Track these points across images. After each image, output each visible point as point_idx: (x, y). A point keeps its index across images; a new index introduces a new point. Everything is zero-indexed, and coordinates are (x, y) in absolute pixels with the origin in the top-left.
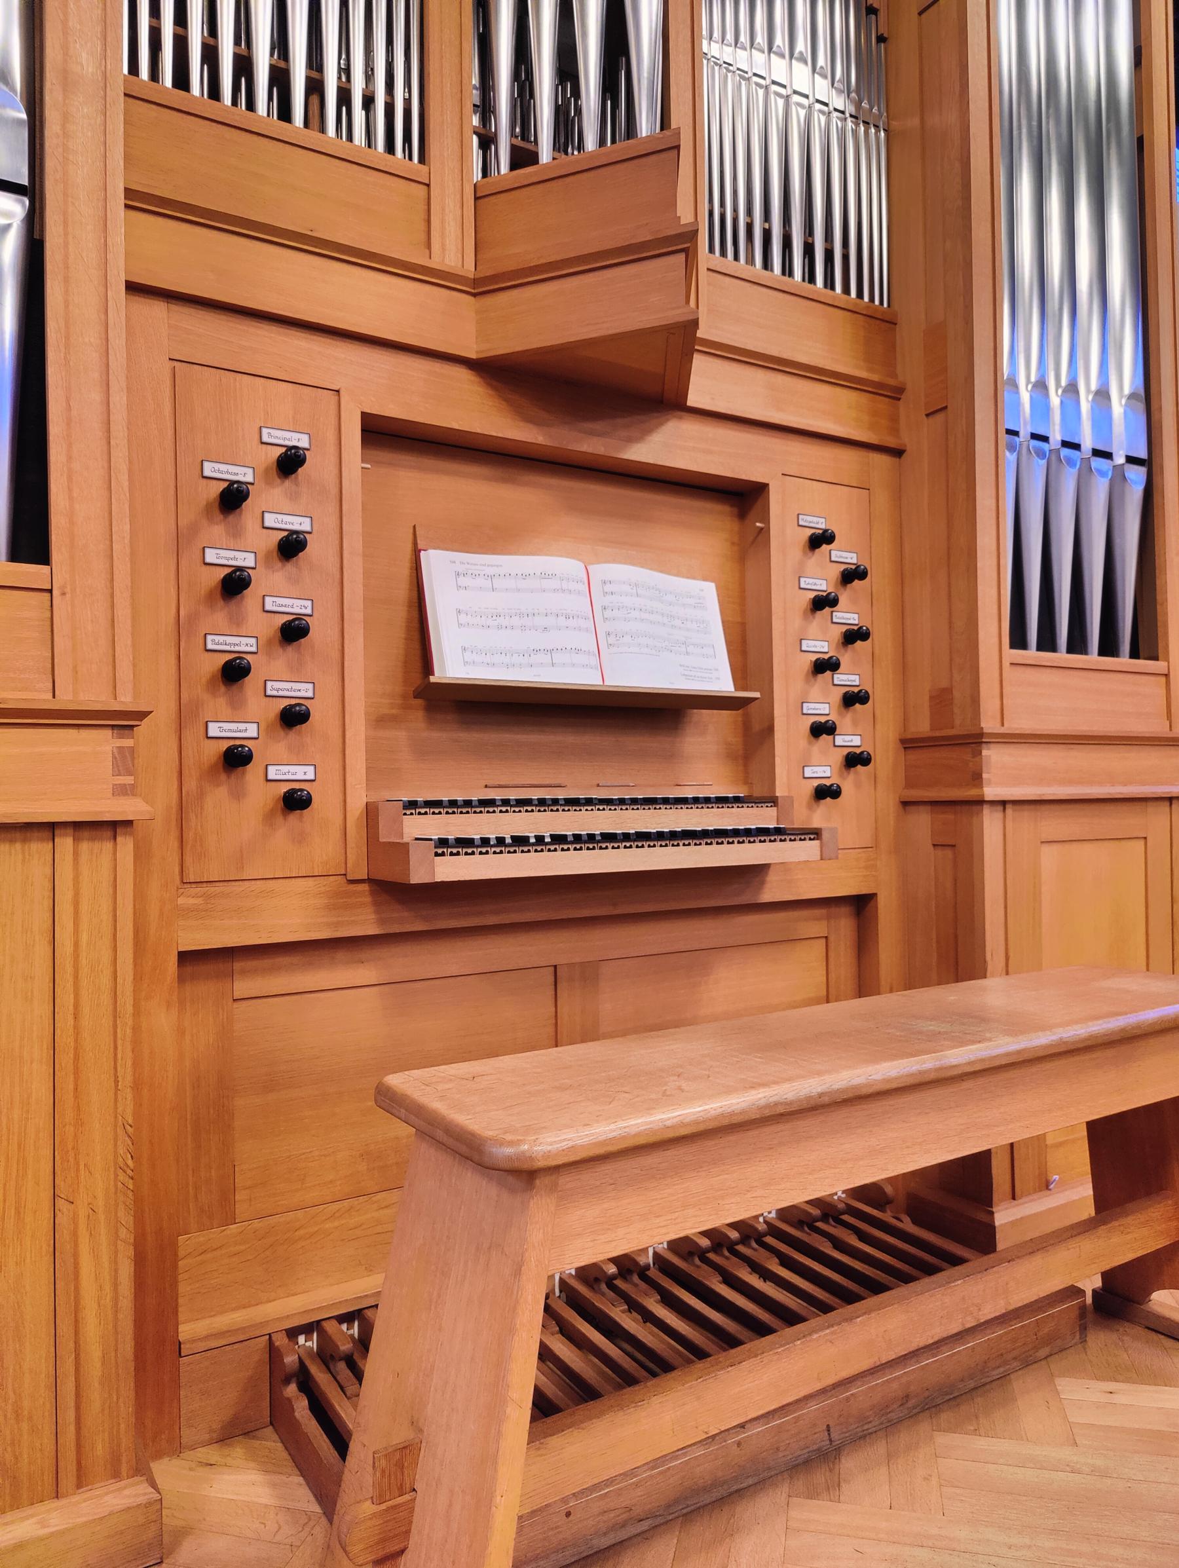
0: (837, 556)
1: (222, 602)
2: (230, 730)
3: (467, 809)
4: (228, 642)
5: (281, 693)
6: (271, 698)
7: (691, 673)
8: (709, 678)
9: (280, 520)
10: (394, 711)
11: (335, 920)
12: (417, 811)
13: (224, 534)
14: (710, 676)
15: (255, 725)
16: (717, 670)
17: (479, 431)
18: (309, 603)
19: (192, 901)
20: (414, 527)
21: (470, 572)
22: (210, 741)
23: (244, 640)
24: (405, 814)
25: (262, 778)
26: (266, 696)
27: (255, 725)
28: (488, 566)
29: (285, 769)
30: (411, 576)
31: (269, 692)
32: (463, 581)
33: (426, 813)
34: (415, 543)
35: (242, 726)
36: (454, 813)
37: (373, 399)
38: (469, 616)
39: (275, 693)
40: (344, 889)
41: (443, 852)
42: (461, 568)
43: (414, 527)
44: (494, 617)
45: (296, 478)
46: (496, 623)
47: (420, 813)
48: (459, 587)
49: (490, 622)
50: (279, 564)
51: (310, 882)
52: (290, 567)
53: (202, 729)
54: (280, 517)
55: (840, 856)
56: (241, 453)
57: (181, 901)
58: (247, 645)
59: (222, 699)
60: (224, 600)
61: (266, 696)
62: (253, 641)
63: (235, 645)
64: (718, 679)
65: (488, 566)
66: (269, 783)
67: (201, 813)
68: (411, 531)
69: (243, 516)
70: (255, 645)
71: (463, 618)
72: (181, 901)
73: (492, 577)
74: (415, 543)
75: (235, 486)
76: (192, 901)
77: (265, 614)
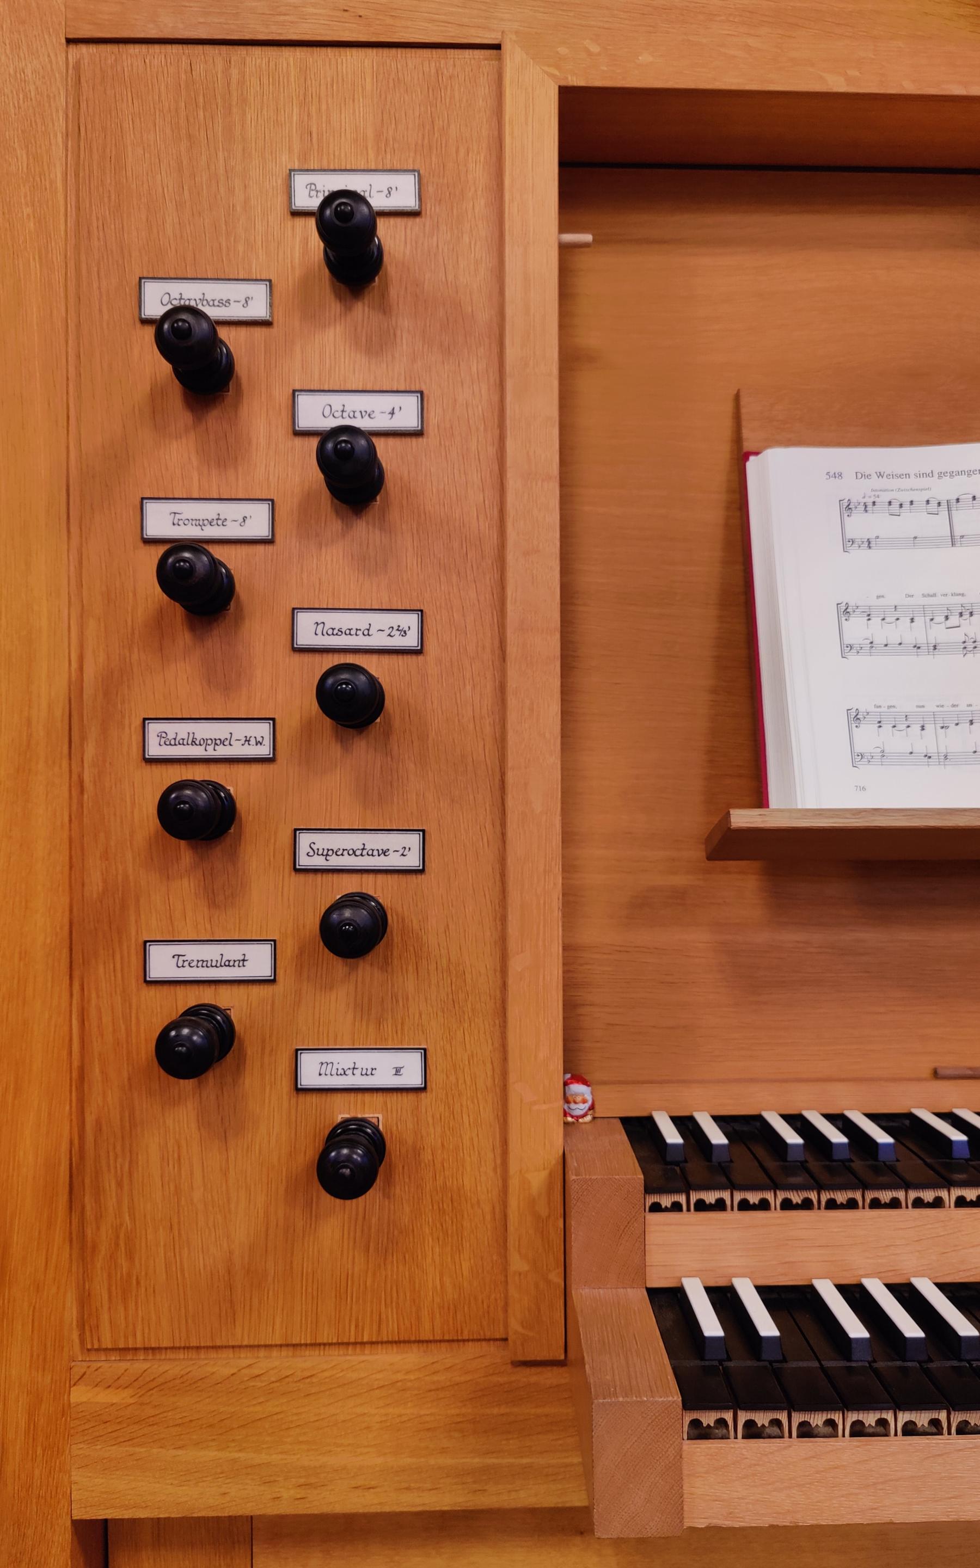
1: (188, 636)
2: (204, 963)
3: (851, 1194)
4: (198, 737)
5: (335, 862)
6: (311, 877)
9: (337, 407)
10: (679, 880)
11: (477, 1461)
12: (694, 1197)
13: (195, 463)
15: (267, 949)
17: (909, 87)
18: (411, 621)
19: (105, 1397)
20: (737, 398)
21: (885, 497)
22: (153, 992)
23: (241, 730)
24: (656, 1208)
25: (285, 1085)
26: (297, 871)
27: (267, 949)
28: (941, 475)
29: (343, 1059)
30: (727, 526)
31: (304, 861)
32: (859, 525)
33: (720, 1205)
34: (738, 439)
35: (233, 951)
36: (807, 1205)
37: (595, 49)
38: (876, 621)
39: (318, 862)
40: (501, 1379)
41: (722, 1422)
42: (857, 491)
43: (737, 398)
44: (954, 620)
45: (384, 295)
46: (957, 636)
47: (701, 1206)
48: (848, 543)
49: (939, 633)
50: (336, 525)
51: (411, 1358)
52: (362, 529)
53: (135, 961)
54: (337, 401)
55: (500, 33)
56: (241, 248)
57: (79, 1395)
58: (247, 741)
59: (185, 882)
60: (192, 628)
61: (297, 871)
62: (263, 730)
63: (217, 742)
65: (941, 475)
66: (302, 1097)
67: (130, 1174)
68: (729, 407)
69: (244, 410)
70: (267, 742)
71: (856, 629)
72: (79, 1395)
73: (951, 506)
74: (738, 439)
75: (166, 326)
76: (105, 1397)
77: (297, 657)
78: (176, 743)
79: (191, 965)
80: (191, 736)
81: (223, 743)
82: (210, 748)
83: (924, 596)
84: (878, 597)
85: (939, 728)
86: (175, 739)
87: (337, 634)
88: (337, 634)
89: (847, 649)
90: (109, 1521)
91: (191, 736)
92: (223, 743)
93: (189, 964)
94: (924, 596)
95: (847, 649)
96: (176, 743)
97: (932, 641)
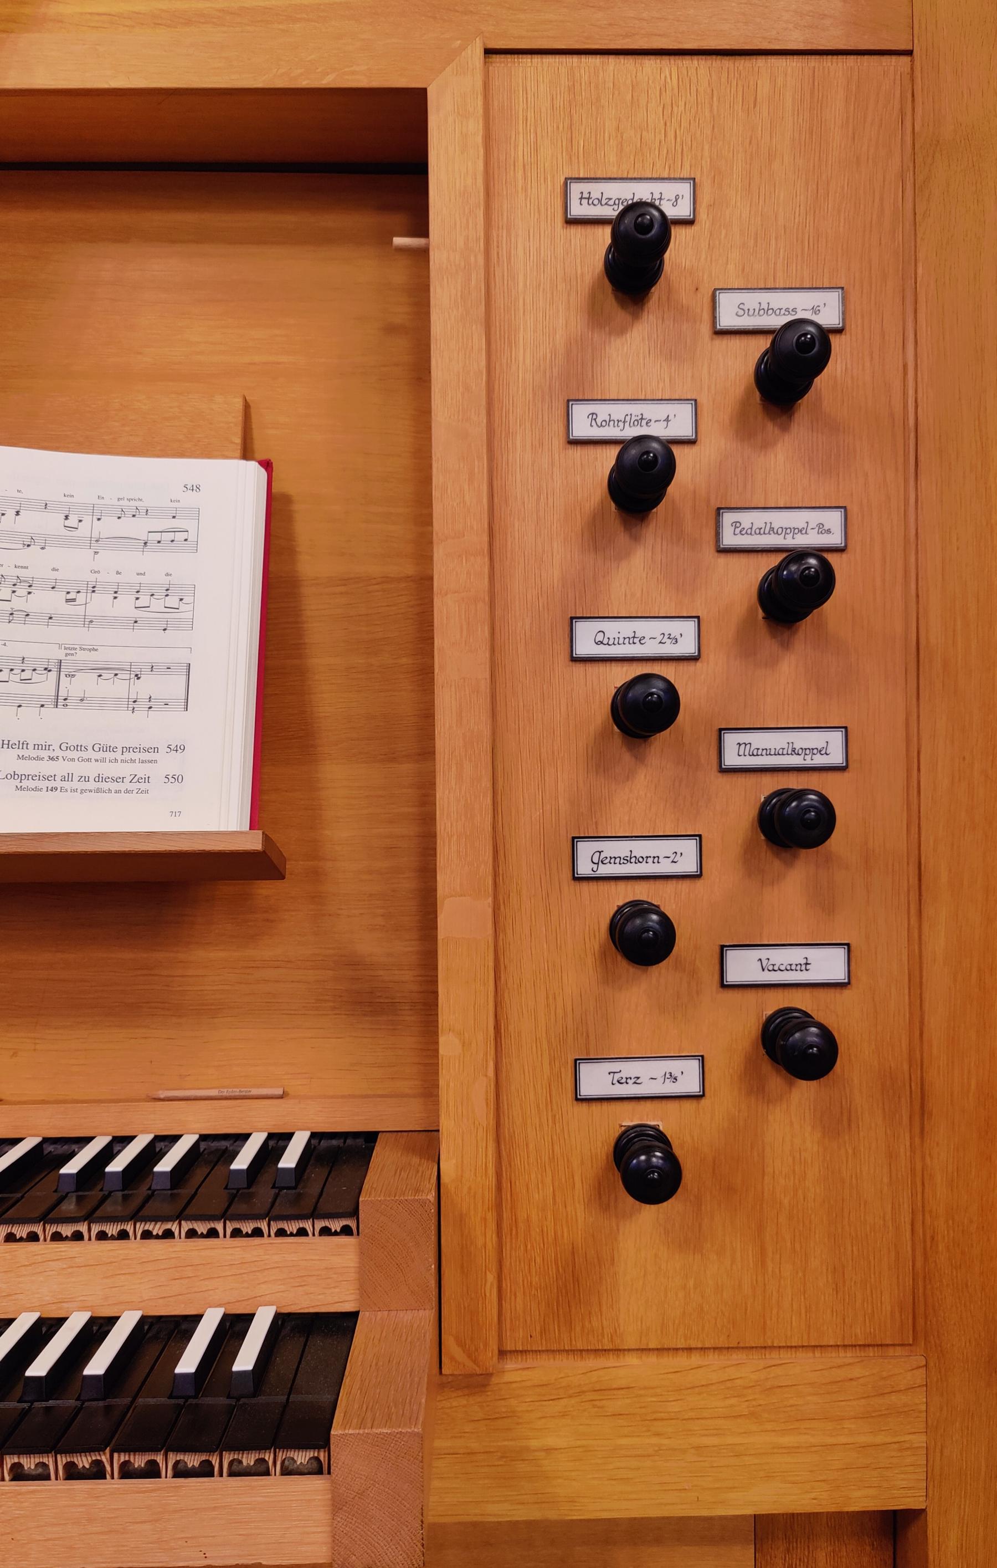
0: (742, 310)
7: (46, 768)
8: (134, 778)
14: (141, 770)
16: (179, 749)
64: (177, 779)
78: (750, 532)
79: (642, 642)
80: (768, 525)
81: (800, 531)
82: (789, 537)
83: (156, 761)
84: (119, 499)
85: (95, 519)
86: (751, 528)
87: (784, 314)
88: (784, 314)
89: (35, 745)
90: (238, 453)
91: (768, 525)
92: (800, 531)
93: (640, 641)
94: (156, 761)
95: (35, 745)
96: (750, 532)
97: (133, 696)
